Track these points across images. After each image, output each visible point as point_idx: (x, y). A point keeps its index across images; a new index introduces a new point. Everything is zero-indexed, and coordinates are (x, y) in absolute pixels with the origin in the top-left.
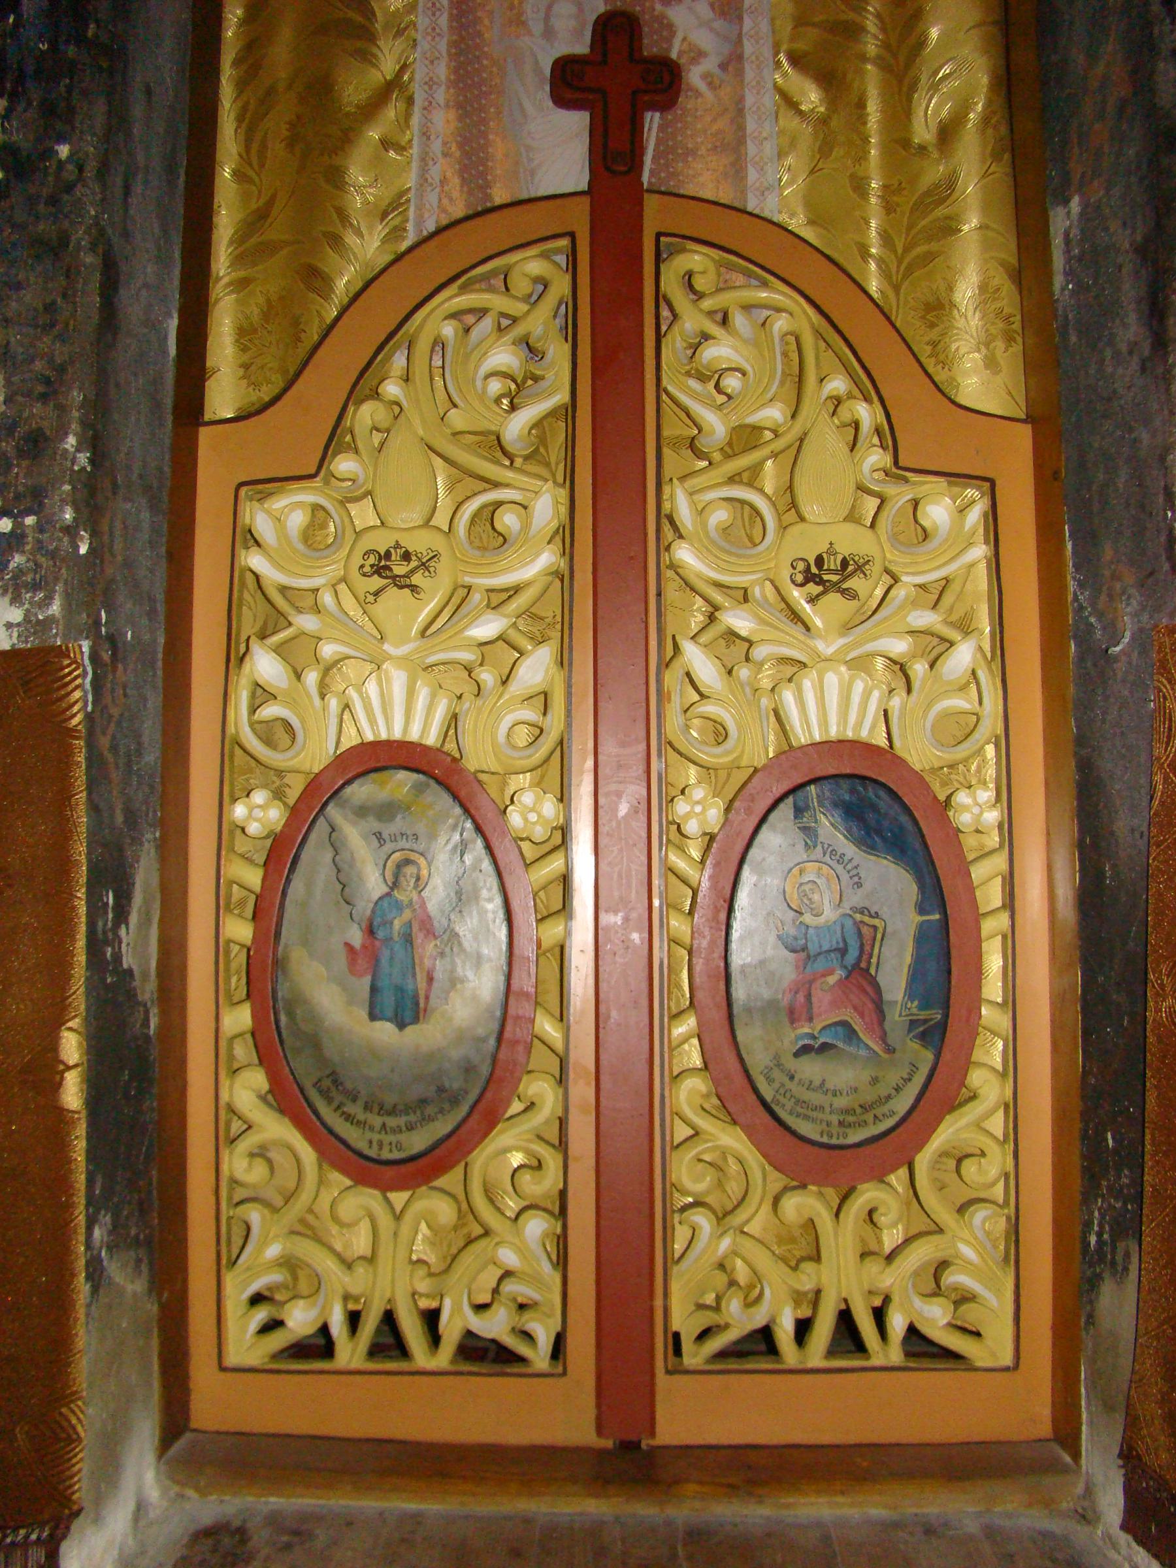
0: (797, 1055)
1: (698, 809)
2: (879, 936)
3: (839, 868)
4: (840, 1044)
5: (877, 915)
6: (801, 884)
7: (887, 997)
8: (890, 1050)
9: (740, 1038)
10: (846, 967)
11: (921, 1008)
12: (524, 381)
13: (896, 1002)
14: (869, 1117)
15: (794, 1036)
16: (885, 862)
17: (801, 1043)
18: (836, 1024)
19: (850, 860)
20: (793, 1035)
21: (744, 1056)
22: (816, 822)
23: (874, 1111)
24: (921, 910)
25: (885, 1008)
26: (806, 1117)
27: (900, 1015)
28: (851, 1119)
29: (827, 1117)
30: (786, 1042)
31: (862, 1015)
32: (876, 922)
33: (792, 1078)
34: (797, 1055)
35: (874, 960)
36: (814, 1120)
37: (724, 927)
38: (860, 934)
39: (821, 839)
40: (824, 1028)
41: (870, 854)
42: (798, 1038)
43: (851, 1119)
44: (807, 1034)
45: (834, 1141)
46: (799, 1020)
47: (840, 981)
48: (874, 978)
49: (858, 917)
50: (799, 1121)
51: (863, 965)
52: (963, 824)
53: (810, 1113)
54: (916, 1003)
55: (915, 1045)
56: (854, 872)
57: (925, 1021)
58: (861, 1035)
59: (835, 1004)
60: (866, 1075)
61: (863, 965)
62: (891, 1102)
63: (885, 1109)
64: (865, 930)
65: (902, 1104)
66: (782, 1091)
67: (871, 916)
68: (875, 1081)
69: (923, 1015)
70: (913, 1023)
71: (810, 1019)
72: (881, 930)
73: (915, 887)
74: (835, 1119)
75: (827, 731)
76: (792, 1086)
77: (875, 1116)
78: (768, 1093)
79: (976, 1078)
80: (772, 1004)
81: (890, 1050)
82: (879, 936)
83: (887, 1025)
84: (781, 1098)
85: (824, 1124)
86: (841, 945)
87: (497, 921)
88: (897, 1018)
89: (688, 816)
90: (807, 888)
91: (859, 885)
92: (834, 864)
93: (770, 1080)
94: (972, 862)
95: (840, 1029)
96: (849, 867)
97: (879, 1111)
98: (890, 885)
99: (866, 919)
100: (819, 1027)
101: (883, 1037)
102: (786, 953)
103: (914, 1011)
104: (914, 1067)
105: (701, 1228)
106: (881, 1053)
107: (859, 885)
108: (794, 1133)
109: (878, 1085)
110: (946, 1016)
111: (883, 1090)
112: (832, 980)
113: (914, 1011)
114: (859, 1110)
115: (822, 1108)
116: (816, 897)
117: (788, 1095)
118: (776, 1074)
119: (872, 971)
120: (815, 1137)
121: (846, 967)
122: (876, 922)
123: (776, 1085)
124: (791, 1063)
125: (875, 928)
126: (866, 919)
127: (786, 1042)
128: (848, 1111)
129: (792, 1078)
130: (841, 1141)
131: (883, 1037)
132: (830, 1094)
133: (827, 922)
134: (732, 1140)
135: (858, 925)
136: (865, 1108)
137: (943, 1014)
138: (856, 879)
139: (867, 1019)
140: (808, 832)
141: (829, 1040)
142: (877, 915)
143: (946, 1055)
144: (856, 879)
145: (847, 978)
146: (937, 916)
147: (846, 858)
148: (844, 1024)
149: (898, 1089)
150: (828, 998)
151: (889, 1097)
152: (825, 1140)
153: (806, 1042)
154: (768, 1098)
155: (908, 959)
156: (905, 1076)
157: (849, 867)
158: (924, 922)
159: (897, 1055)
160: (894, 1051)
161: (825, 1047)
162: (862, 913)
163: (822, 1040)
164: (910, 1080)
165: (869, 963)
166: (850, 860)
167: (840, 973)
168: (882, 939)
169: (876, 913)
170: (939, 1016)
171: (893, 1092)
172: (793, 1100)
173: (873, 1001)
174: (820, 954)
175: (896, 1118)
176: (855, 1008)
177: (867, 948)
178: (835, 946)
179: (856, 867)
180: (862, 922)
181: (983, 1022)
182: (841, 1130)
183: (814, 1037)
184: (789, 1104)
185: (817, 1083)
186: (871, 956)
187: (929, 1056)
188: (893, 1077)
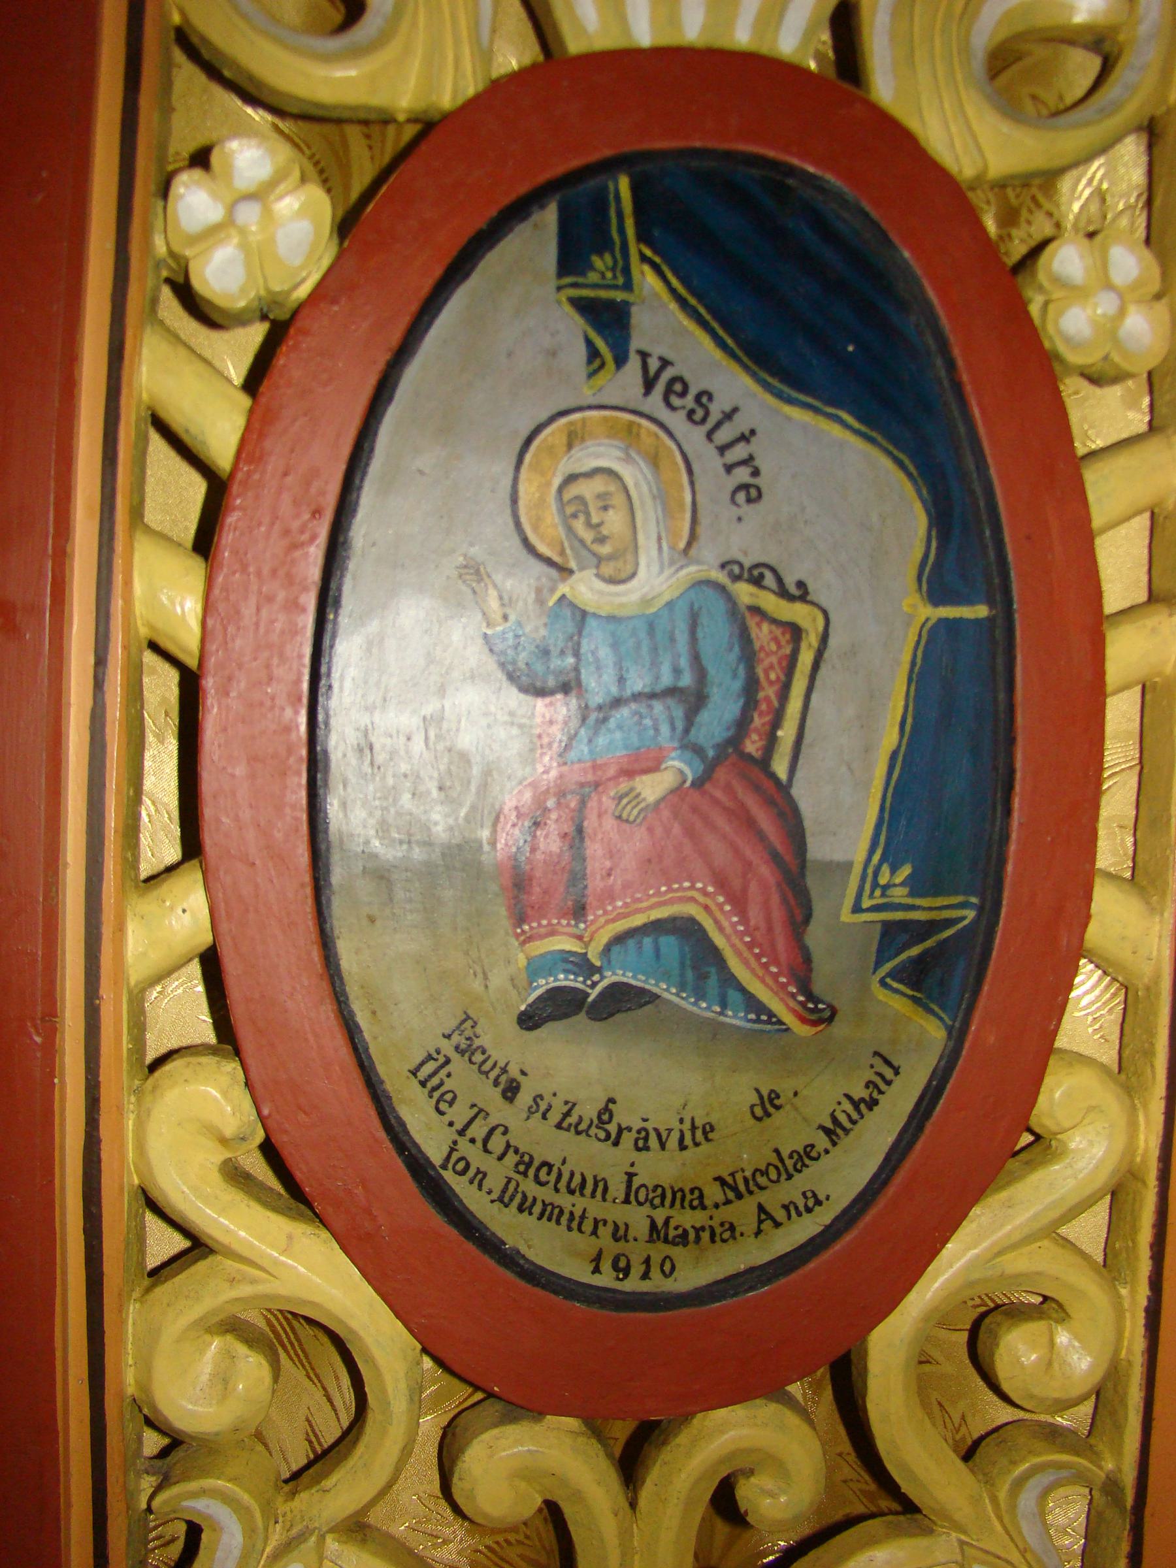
0: (529, 1020)
1: (249, 214)
2: (806, 658)
3: (693, 438)
4: (667, 991)
5: (802, 594)
6: (571, 479)
7: (819, 849)
8: (820, 1014)
9: (348, 961)
10: (698, 750)
11: (916, 886)
12: (767, 1169)
13: (848, 866)
14: (744, 1213)
15: (512, 968)
16: (836, 430)
17: (543, 984)
18: (656, 927)
19: (728, 416)
20: (522, 961)
21: (362, 1019)
22: (628, 286)
23: (762, 1197)
24: (938, 589)
25: (811, 881)
26: (551, 1213)
27: (857, 909)
28: (688, 1219)
29: (617, 1213)
30: (498, 979)
31: (739, 902)
32: (797, 612)
33: (511, 1091)
34: (529, 1020)
35: (787, 734)
36: (576, 1222)
37: (310, 601)
38: (749, 655)
39: (636, 344)
40: (620, 939)
41: (790, 401)
42: (536, 968)
43: (688, 1219)
44: (565, 956)
45: (632, 1284)
46: (541, 910)
47: (677, 791)
48: (784, 789)
49: (744, 592)
50: (528, 1221)
51: (753, 746)
52: (1067, 340)
53: (564, 1200)
54: (906, 871)
55: (895, 1002)
56: (739, 452)
57: (933, 927)
58: (735, 965)
59: (659, 867)
60: (742, 1092)
61: (753, 746)
62: (814, 1167)
63: (791, 1191)
64: (762, 634)
65: (844, 1175)
66: (478, 1130)
67: (783, 593)
68: (768, 1104)
69: (924, 909)
70: (894, 935)
71: (579, 911)
72: (811, 640)
73: (920, 520)
74: (637, 1218)
75: (674, 19)
76: (510, 1115)
77: (761, 1208)
78: (431, 1138)
79: (1060, 1096)
80: (459, 858)
81: (820, 1014)
82: (806, 658)
83: (816, 936)
84: (474, 1154)
85: (605, 1232)
86: (687, 680)
87: (340, 755)
88: (846, 916)
89: (213, 233)
90: (587, 489)
91: (751, 493)
92: (676, 421)
93: (442, 1100)
94: (1092, 454)
95: (670, 944)
96: (725, 435)
97: (774, 1198)
98: (841, 502)
99: (770, 602)
100: (604, 937)
101: (801, 973)
102: (513, 697)
103: (899, 894)
104: (888, 1066)
105: (217, 1528)
106: (789, 1019)
107: (751, 493)
108: (509, 1259)
109: (778, 1117)
110: (990, 910)
111: (790, 1132)
112: (652, 787)
113: (899, 894)
114: (714, 1193)
115: (601, 1187)
116: (614, 522)
117: (497, 1144)
118: (462, 1078)
119: (780, 768)
120: (579, 1272)
121: (698, 750)
122: (797, 612)
123: (460, 1113)
124: (506, 1044)
125: (795, 632)
126: (770, 602)
127: (498, 979)
128: (678, 1196)
129: (511, 1091)
130: (657, 1284)
131: (801, 973)
132: (628, 1139)
133: (646, 601)
134: (311, 1269)
135: (742, 620)
136: (733, 1187)
137: (980, 909)
138: (742, 475)
139: (755, 914)
140: (608, 320)
141: (628, 978)
142: (802, 594)
143: (983, 1031)
144: (742, 475)
145: (698, 784)
146: (981, 611)
147: (716, 410)
148: (686, 930)
149: (833, 1131)
150: (638, 842)
151: (807, 1155)
152: (606, 1279)
153: (563, 980)
154: (435, 1152)
155: (890, 739)
156: (859, 1092)
157: (725, 435)
158: (943, 621)
159: (839, 1029)
160: (832, 1016)
161: (620, 1000)
162: (757, 582)
163: (610, 978)
164: (872, 1104)
165: (771, 741)
166: (728, 416)
167: (677, 768)
168: (816, 666)
169: (801, 584)
170: (971, 914)
171: (822, 1142)
172: (511, 1159)
173: (775, 858)
174: (617, 702)
175: (824, 1217)
176: (722, 884)
177: (769, 692)
178: (666, 680)
179: (744, 438)
180: (756, 610)
181: (1093, 934)
182: (658, 1251)
183: (584, 966)
184: (498, 1173)
185: (588, 1111)
186: (777, 722)
187: (934, 1032)
188: (823, 1093)
